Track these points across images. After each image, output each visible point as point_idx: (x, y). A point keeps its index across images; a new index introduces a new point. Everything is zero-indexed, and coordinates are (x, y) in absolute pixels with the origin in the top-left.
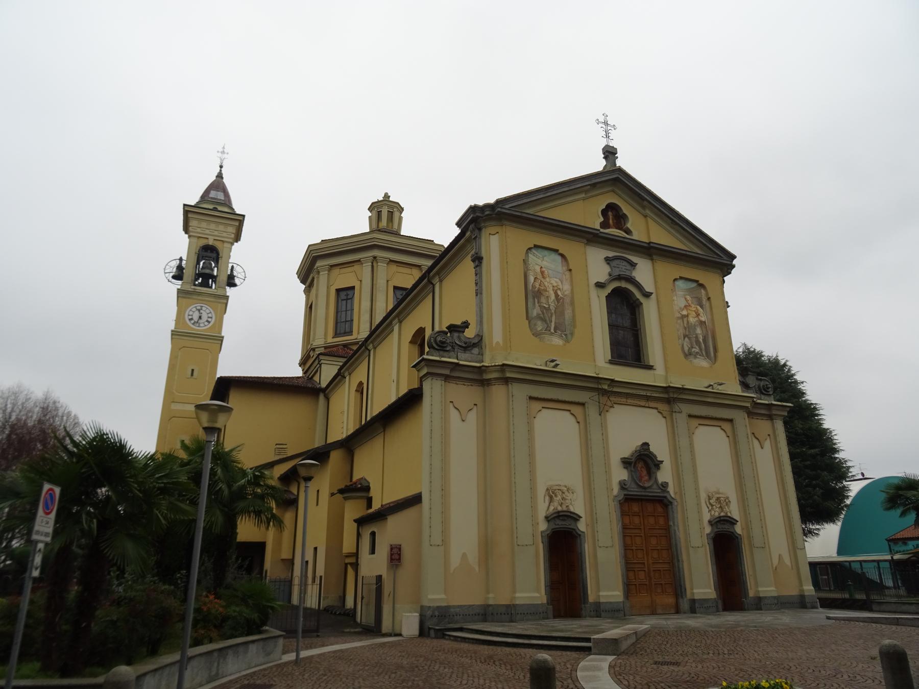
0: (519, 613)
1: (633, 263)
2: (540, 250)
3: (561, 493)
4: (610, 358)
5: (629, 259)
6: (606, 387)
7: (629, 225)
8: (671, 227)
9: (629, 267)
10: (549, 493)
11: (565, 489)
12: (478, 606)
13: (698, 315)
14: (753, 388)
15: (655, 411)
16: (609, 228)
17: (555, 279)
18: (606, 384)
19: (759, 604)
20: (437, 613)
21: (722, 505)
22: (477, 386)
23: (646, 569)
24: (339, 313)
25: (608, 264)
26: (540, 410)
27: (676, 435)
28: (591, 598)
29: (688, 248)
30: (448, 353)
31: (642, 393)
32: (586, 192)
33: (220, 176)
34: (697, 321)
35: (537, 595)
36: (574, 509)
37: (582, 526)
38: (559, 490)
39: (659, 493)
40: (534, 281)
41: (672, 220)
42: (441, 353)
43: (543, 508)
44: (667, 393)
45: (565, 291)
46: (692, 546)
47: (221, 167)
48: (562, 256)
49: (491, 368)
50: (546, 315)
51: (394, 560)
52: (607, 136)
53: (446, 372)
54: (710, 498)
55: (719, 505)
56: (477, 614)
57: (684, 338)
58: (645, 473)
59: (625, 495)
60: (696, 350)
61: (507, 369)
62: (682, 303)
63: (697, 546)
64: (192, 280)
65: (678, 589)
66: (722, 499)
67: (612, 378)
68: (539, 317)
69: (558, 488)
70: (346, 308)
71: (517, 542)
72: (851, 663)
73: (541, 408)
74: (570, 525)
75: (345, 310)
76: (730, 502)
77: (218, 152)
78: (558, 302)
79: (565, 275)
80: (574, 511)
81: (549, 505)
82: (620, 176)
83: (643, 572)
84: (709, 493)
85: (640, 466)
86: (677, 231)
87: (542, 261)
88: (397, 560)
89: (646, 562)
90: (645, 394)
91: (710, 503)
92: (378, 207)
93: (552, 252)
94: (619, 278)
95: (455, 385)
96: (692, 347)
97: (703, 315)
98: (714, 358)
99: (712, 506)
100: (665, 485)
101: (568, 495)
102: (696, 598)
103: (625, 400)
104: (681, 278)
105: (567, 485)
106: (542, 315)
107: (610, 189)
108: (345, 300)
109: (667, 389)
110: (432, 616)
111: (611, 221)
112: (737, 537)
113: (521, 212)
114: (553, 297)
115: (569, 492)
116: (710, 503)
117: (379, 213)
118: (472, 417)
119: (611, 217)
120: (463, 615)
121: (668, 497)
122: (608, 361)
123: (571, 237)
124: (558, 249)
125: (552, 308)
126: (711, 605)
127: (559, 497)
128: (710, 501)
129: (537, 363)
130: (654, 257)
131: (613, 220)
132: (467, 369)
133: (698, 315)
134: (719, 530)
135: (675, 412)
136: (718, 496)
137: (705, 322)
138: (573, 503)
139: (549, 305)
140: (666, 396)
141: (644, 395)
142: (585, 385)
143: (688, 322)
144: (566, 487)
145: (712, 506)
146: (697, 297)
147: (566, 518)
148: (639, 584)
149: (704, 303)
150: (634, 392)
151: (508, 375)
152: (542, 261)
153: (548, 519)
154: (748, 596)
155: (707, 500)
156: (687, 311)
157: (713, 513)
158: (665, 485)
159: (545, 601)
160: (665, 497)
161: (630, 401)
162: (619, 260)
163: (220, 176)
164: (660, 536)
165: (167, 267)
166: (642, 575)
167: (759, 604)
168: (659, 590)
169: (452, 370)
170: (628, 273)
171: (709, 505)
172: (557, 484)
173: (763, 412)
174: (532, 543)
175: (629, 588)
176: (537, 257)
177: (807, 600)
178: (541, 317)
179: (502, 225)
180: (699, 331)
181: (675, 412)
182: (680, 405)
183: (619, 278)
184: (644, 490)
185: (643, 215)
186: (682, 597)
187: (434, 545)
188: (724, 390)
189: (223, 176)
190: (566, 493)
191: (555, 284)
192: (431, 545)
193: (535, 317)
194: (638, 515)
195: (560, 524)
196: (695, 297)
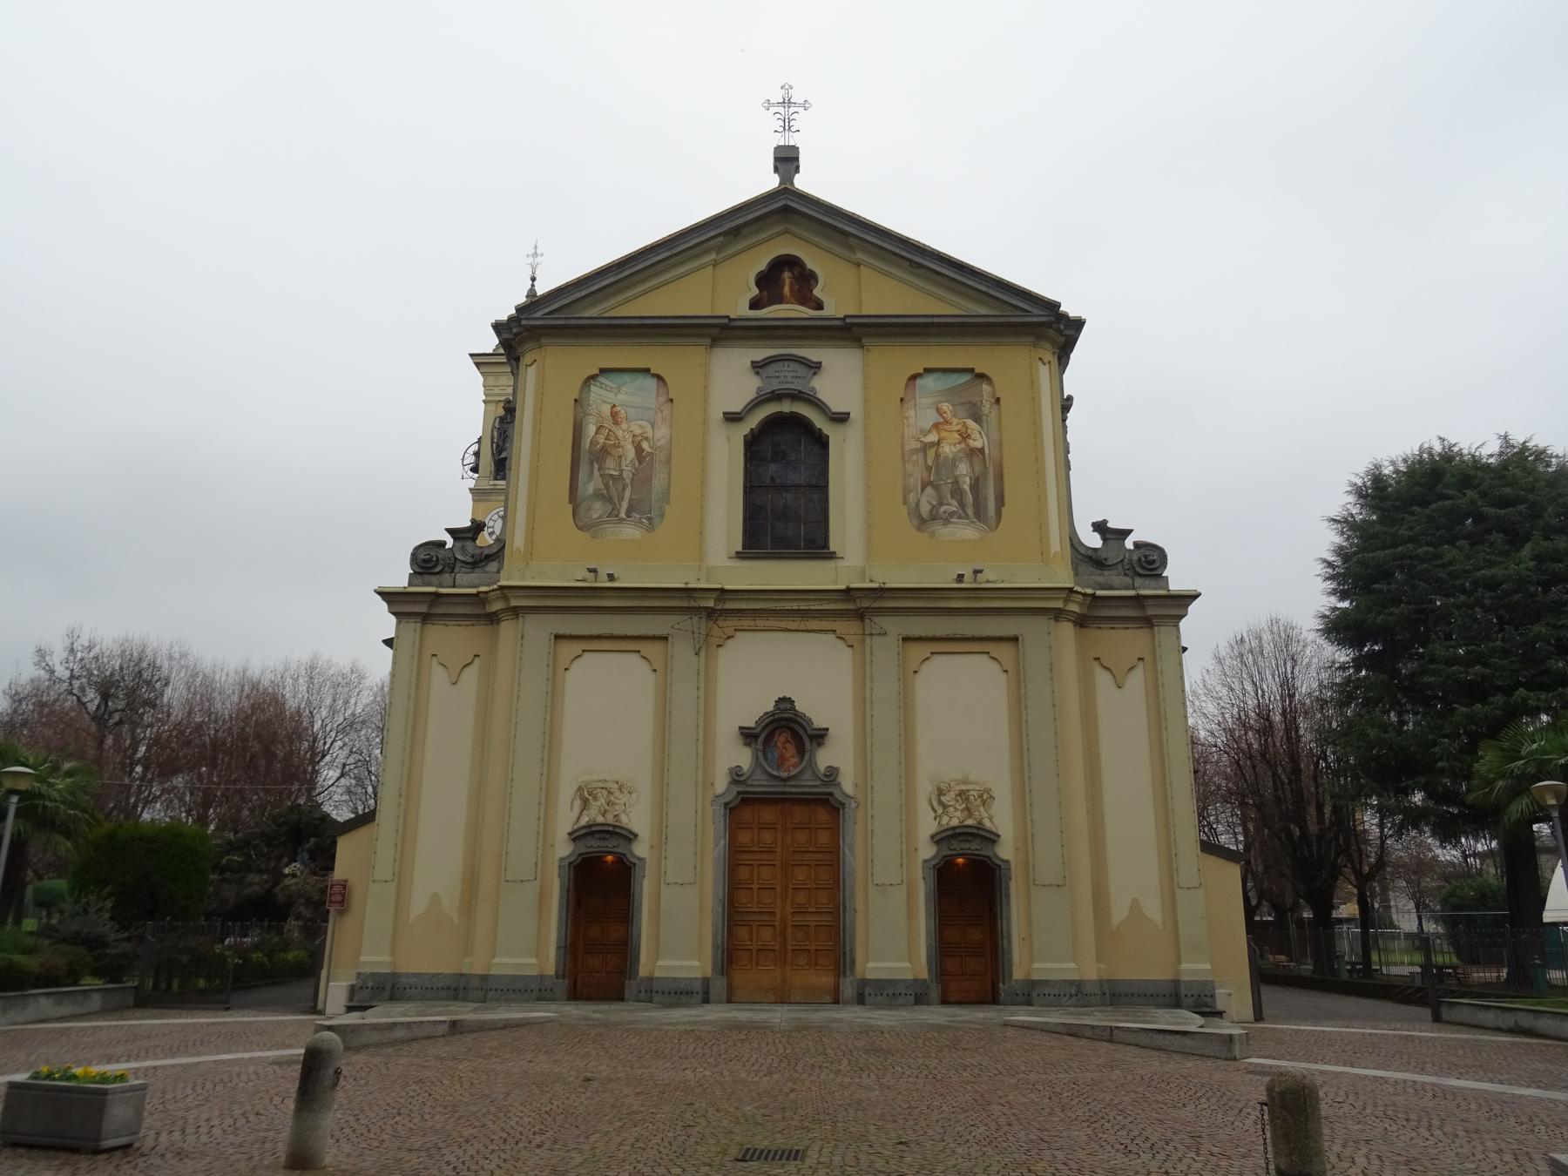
2: (613, 376)
5: (800, 357)
6: (711, 604)
8: (913, 274)
9: (801, 370)
11: (616, 786)
12: (448, 975)
13: (965, 436)
14: (1120, 567)
15: (831, 637)
16: (781, 303)
19: (1030, 994)
20: (370, 984)
21: (970, 805)
25: (757, 373)
28: (643, 971)
29: (959, 309)
32: (719, 249)
35: (696, 963)
37: (641, 849)
38: (602, 788)
39: (816, 786)
40: (596, 433)
43: (566, 818)
45: (658, 440)
46: (875, 882)
47: (533, 279)
48: (659, 378)
49: (491, 594)
50: (612, 488)
53: (423, 608)
54: (940, 793)
55: (964, 805)
56: (660, 991)
59: (739, 793)
60: (953, 506)
61: (509, 593)
62: (930, 417)
64: (491, 471)
67: (719, 586)
68: (598, 495)
69: (601, 785)
71: (505, 876)
76: (992, 797)
77: (528, 256)
78: (639, 462)
80: (629, 827)
81: (581, 815)
82: (789, 203)
85: (782, 739)
87: (616, 395)
88: (339, 902)
90: (796, 608)
91: (941, 803)
93: (639, 375)
96: (941, 504)
97: (978, 436)
99: (945, 806)
102: (868, 977)
104: (928, 371)
106: (605, 491)
109: (848, 590)
110: (361, 988)
111: (787, 290)
113: (566, 318)
114: (631, 453)
115: (621, 792)
118: (471, 676)
119: (787, 281)
120: (422, 988)
121: (836, 793)
125: (627, 475)
127: (602, 801)
128: (943, 798)
130: (865, 341)
131: (791, 286)
132: (457, 600)
135: (871, 634)
136: (964, 787)
137: (982, 450)
138: (628, 810)
139: (621, 471)
140: (851, 606)
143: (937, 455)
144: (617, 783)
145: (945, 806)
146: (970, 402)
149: (986, 410)
150: (772, 605)
151: (514, 603)
152: (616, 395)
153: (576, 837)
156: (938, 433)
157: (945, 820)
158: (832, 773)
159: (551, 971)
160: (831, 794)
161: (761, 623)
162: (782, 363)
164: (816, 865)
165: (467, 455)
167: (1030, 994)
169: (431, 605)
170: (798, 386)
171: (936, 806)
172: (600, 778)
175: (729, 956)
176: (606, 390)
177: (1183, 991)
178: (602, 495)
179: (540, 347)
180: (963, 469)
181: (871, 634)
182: (877, 619)
184: (782, 783)
185: (853, 263)
186: (845, 976)
187: (380, 881)
190: (617, 794)
191: (638, 431)
192: (507, 881)
193: (590, 496)
195: (594, 845)
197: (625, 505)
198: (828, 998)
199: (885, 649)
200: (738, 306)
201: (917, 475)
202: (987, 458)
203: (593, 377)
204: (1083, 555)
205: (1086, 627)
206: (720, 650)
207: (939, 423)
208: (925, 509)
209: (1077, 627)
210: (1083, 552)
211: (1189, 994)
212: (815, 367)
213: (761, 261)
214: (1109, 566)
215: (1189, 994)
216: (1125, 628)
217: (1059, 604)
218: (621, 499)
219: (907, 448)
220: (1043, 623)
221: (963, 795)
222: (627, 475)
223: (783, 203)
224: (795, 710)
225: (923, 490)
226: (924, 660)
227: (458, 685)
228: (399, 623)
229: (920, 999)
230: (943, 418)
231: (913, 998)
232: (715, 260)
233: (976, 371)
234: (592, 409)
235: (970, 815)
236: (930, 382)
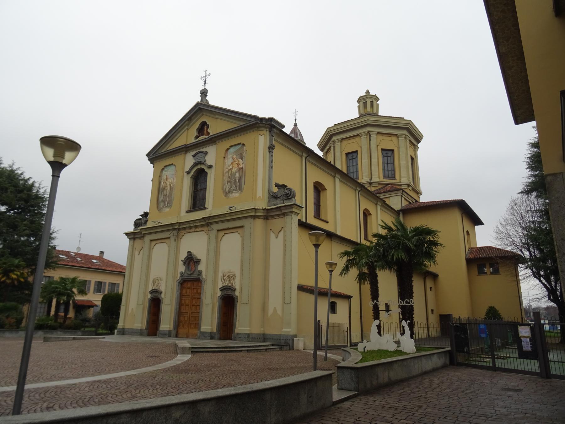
6: (177, 227)
13: (238, 165)
14: (281, 197)
16: (204, 135)
24: (349, 168)
27: (394, 212)
31: (192, 225)
32: (188, 125)
33: (296, 125)
44: (205, 221)
47: (296, 120)
54: (224, 276)
57: (227, 183)
59: (182, 279)
63: (208, 303)
65: (197, 325)
66: (231, 275)
69: (157, 279)
70: (353, 164)
72: (210, 380)
75: (352, 165)
76: (235, 277)
83: (187, 317)
84: (225, 273)
89: (189, 312)
91: (224, 279)
92: (364, 99)
96: (231, 187)
99: (224, 280)
103: (185, 231)
104: (231, 147)
107: (200, 115)
108: (351, 159)
116: (224, 279)
117: (365, 103)
127: (157, 283)
136: (229, 274)
145: (224, 280)
155: (222, 277)
158: (200, 273)
161: (198, 230)
163: (296, 125)
168: (192, 326)
173: (277, 213)
188: (241, 209)
189: (297, 125)
197: (167, 202)
198: (185, 336)
199: (213, 233)
200: (192, 140)
201: (226, 179)
202: (243, 170)
203: (163, 169)
204: (271, 195)
205: (269, 219)
206: (182, 239)
207: (233, 162)
208: (227, 189)
209: (265, 220)
210: (271, 195)
211: (283, 339)
212: (206, 153)
213: (197, 125)
214: (279, 197)
215: (283, 339)
216: (279, 218)
217: (253, 214)
218: (166, 201)
219: (225, 172)
220: (251, 220)
221: (229, 276)
222: (168, 194)
223: (198, 107)
224: (192, 255)
225: (227, 183)
226: (154, 246)
227: (278, 238)
228: (130, 241)
229: (212, 338)
230: (234, 160)
231: (210, 337)
232: (187, 128)
233: (242, 143)
234: (163, 178)
235: (230, 283)
236: (232, 150)
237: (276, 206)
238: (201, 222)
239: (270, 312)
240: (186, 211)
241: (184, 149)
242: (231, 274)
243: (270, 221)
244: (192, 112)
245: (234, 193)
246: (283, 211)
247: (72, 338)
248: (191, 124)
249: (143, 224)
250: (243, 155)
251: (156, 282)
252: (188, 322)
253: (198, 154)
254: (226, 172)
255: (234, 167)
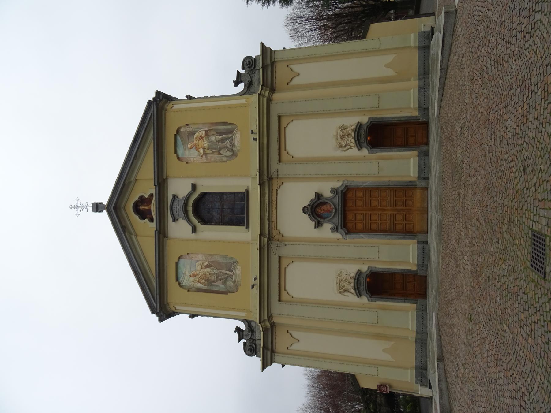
0: (422, 329)
1: (172, 198)
2: (179, 276)
3: (342, 282)
4: (244, 227)
6: (266, 239)
7: (146, 196)
10: (342, 292)
11: (339, 278)
12: (416, 346)
13: (201, 138)
14: (252, 75)
16: (151, 210)
17: (196, 266)
18: (264, 240)
19: (424, 108)
20: (420, 378)
22: (276, 329)
23: (395, 213)
25: (177, 220)
26: (287, 152)
29: (152, 141)
30: (257, 346)
32: (130, 234)
34: (206, 139)
36: (353, 273)
38: (340, 284)
39: (339, 197)
41: (133, 159)
42: (257, 350)
43: (352, 298)
45: (203, 259)
48: (179, 258)
50: (222, 277)
51: (387, 390)
52: (85, 207)
53: (269, 353)
54: (341, 147)
55: (346, 137)
57: (221, 154)
58: (324, 207)
59: (341, 229)
60: (228, 142)
61: (262, 320)
62: (194, 151)
66: (341, 134)
68: (224, 283)
69: (338, 284)
73: (286, 152)
74: (363, 279)
76: (343, 125)
79: (192, 257)
85: (320, 211)
86: (141, 153)
87: (186, 275)
88: (387, 388)
89: (390, 213)
91: (345, 146)
94: (186, 213)
95: (277, 344)
96: (227, 147)
97: (200, 132)
98: (233, 126)
99: (347, 145)
100: (333, 191)
101: (343, 276)
103: (274, 223)
104: (176, 152)
105: (336, 277)
107: (123, 210)
109: (260, 184)
110: (421, 382)
112: (371, 122)
116: (345, 146)
119: (143, 207)
122: (247, 230)
123: (165, 199)
124: (174, 135)
125: (217, 271)
126: (423, 161)
127: (345, 284)
128: (343, 146)
129: (256, 293)
132: (266, 338)
133: (201, 138)
134: (365, 141)
136: (339, 137)
137: (206, 131)
138: (348, 273)
139: (215, 274)
140: (267, 183)
141: (268, 206)
142: (267, 310)
143: (208, 149)
144: (337, 278)
145: (347, 145)
146: (188, 136)
147: (359, 282)
148: (406, 221)
149: (191, 130)
150: (266, 215)
152: (186, 275)
154: (416, 117)
158: (333, 191)
159: (414, 306)
161: (274, 219)
166: (399, 217)
169: (268, 349)
170: (181, 204)
171: (347, 148)
173: (269, 73)
174: (376, 312)
176: (184, 279)
177: (423, 45)
181: (278, 175)
183: (186, 213)
184: (337, 211)
187: (378, 373)
188: (256, 122)
190: (342, 278)
191: (200, 267)
194: (356, 200)
195: (363, 287)
196: (188, 138)
197: (228, 272)
198: (426, 192)
201: (216, 157)
203: (179, 284)
205: (275, 88)
208: (229, 154)
210: (246, 90)
212: (175, 197)
213: (135, 218)
214: (251, 80)
216: (276, 73)
219: (205, 161)
220: (273, 106)
221: (341, 138)
224: (308, 206)
226: (287, 292)
227: (299, 339)
228: (275, 362)
229: (426, 154)
232: (135, 236)
234: (192, 284)
237: (262, 333)
238: (264, 189)
239: (390, 72)
240: (246, 228)
241: (161, 236)
242: (339, 135)
243: (278, 86)
244: (115, 220)
245: (234, 143)
246: (269, 62)
247: (441, 364)
248: (131, 229)
249: (252, 338)
250: (190, 132)
251: (344, 286)
252: (405, 213)
253: (173, 210)
254: (207, 158)
255: (202, 146)
